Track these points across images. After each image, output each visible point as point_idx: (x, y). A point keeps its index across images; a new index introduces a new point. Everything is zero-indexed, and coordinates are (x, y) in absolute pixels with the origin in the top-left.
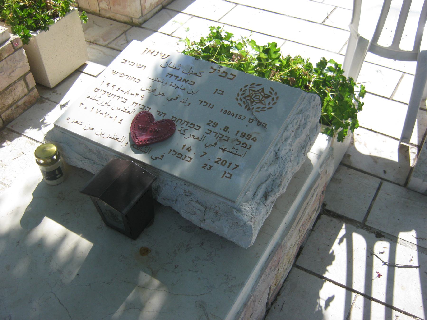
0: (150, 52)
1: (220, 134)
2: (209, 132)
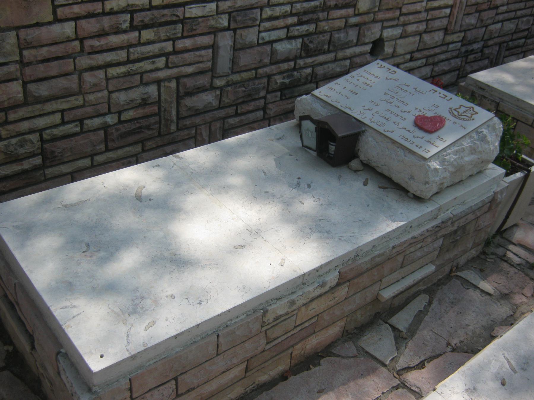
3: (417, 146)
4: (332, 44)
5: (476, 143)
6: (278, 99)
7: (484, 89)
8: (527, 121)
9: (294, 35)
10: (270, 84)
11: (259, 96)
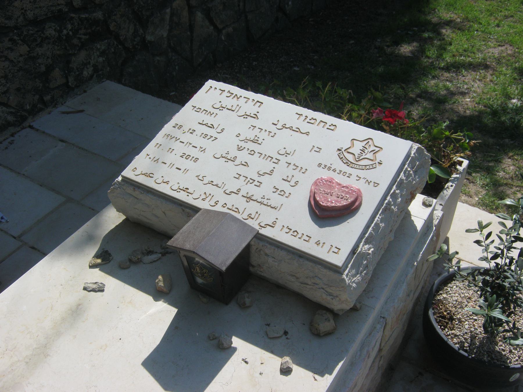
0: (209, 114)
1: (251, 179)
2: (237, 176)
3: (318, 243)
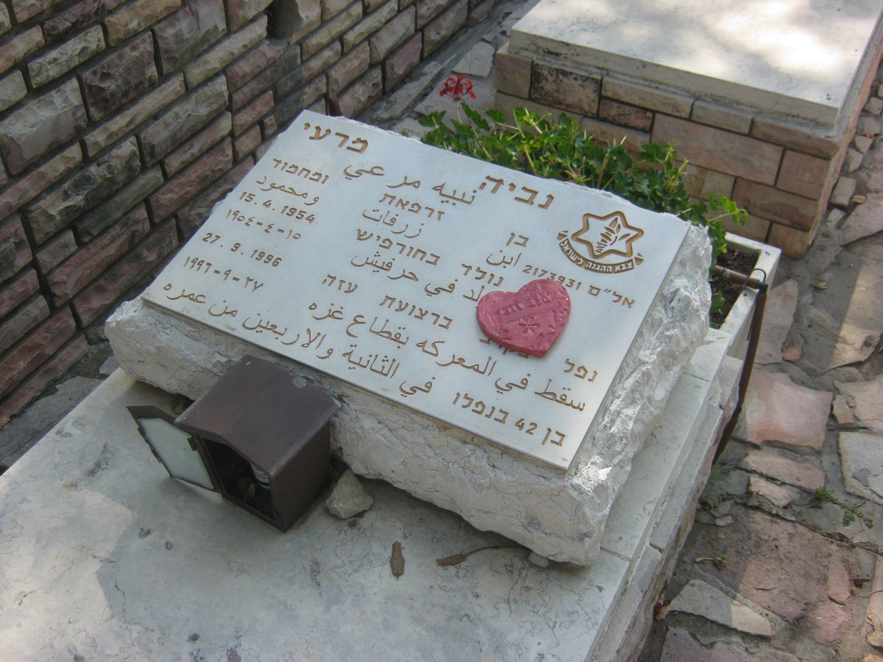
4: (164, 56)
5: (670, 338)
6: (74, 248)
7: (557, 54)
8: (678, 111)
9: (50, 79)
10: (34, 226)
11: (16, 270)
